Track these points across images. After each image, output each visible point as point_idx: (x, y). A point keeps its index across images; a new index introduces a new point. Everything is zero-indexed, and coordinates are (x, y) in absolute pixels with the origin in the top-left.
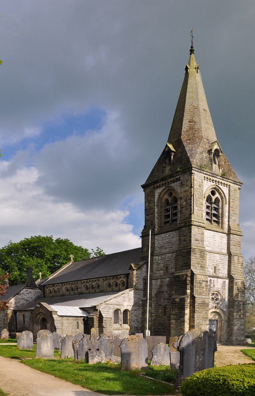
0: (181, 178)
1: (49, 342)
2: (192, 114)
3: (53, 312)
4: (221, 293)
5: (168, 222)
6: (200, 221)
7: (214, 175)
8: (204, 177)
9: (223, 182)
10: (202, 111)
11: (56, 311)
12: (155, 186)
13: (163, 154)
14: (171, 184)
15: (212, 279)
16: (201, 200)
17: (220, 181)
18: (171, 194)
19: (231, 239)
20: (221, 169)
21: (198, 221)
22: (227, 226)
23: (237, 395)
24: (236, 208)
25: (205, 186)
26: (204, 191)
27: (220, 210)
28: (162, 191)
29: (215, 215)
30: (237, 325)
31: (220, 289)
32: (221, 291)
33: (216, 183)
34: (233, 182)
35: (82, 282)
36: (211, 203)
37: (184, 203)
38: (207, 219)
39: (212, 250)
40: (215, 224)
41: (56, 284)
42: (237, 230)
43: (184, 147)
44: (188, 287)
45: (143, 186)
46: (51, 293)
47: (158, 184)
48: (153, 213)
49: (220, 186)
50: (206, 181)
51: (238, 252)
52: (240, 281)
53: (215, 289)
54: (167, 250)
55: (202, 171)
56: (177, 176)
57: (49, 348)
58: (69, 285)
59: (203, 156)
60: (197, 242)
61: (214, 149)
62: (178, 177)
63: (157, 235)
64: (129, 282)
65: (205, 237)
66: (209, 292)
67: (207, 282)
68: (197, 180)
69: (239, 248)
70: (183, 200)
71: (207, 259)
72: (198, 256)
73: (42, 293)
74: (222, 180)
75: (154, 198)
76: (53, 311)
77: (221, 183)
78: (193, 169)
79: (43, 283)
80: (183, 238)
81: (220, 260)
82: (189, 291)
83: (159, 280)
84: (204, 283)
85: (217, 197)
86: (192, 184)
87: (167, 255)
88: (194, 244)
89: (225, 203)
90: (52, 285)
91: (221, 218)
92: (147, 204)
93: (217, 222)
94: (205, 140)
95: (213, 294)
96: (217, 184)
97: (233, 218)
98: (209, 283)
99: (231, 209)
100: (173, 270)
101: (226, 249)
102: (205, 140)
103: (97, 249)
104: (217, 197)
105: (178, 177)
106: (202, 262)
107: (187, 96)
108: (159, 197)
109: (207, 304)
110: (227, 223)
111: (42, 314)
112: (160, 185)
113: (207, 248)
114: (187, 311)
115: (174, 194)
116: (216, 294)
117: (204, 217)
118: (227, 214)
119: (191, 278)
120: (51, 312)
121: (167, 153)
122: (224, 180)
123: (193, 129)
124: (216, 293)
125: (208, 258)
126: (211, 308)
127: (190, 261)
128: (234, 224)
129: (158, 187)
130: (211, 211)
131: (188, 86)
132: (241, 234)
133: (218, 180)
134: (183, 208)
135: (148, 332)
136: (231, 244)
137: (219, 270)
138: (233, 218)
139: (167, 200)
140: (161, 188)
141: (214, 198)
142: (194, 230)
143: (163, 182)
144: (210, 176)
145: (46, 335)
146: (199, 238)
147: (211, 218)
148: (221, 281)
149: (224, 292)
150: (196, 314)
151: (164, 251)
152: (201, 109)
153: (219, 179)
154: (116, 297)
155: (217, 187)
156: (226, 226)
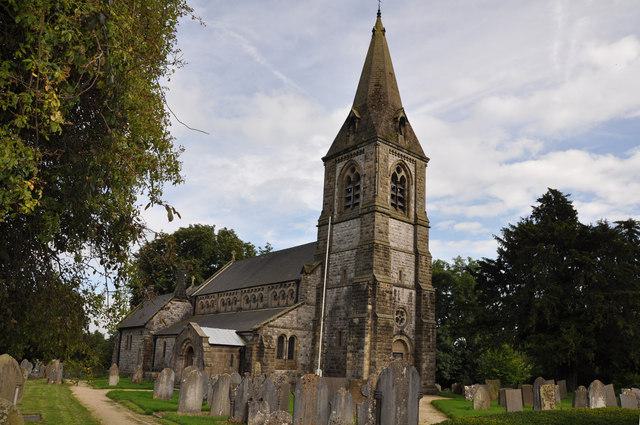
1: (198, 385)
9: (410, 156)
40: (400, 211)
45: (324, 159)
84: (388, 295)
100: (352, 275)
113: (391, 244)
118: (413, 198)
120: (202, 337)
129: (340, 161)
139: (349, 177)
142: (379, 218)
148: (407, 291)
151: (343, 247)
156: (412, 214)
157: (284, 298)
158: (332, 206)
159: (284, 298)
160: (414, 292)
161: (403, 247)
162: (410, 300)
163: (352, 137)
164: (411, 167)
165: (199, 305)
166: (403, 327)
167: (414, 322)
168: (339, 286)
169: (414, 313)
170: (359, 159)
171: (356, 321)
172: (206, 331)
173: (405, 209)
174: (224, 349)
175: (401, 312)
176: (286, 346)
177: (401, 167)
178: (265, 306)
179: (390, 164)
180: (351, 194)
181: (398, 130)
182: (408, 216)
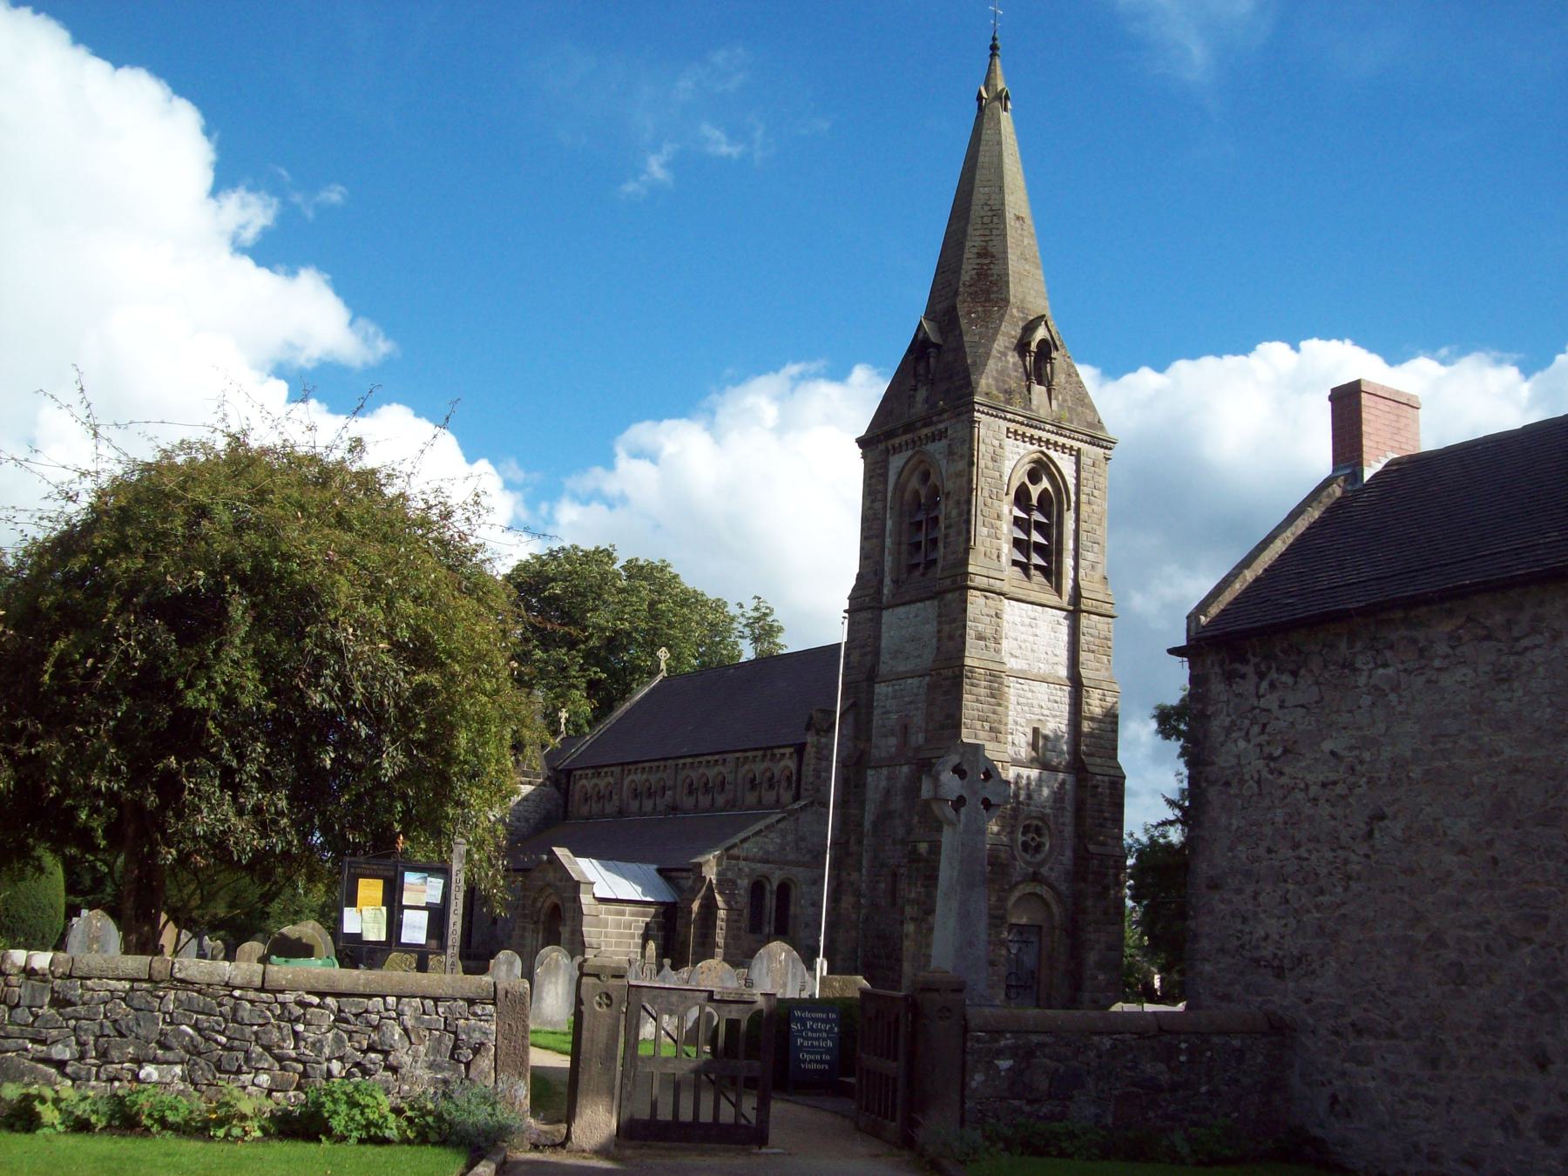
0: (949, 432)
1: (560, 981)
2: (987, 232)
3: (582, 886)
4: (1051, 824)
5: (918, 565)
6: (992, 573)
7: (1035, 423)
8: (1008, 429)
9: (1061, 440)
10: (1012, 223)
11: (592, 880)
12: (890, 443)
13: (911, 350)
14: (926, 444)
17: (1053, 438)
18: (926, 477)
19: (1083, 629)
20: (1057, 399)
21: (985, 572)
24: (1098, 522)
25: (1010, 456)
26: (1007, 472)
28: (906, 463)
31: (1048, 811)
32: (1051, 818)
33: (1040, 446)
34: (1088, 439)
35: (680, 766)
36: (1027, 508)
37: (954, 513)
38: (1015, 563)
39: (1025, 667)
41: (605, 766)
42: (1100, 597)
43: (961, 335)
45: (862, 442)
46: (586, 800)
47: (897, 441)
49: (1051, 453)
51: (1103, 674)
52: (1106, 779)
55: (1001, 414)
56: (940, 422)
57: (560, 1000)
58: (642, 773)
59: (1007, 362)
60: (982, 643)
61: (1037, 340)
62: (941, 426)
63: (887, 608)
64: (803, 777)
65: (1005, 624)
66: (1012, 821)
68: (987, 440)
69: (1105, 658)
70: (951, 502)
71: (1012, 701)
72: (983, 691)
73: (560, 801)
74: (1057, 434)
76: (582, 880)
77: (1056, 444)
79: (567, 761)
80: (946, 628)
83: (885, 771)
85: (1046, 490)
86: (973, 455)
87: (910, 681)
88: (974, 656)
89: (1065, 507)
90: (592, 771)
94: (1015, 311)
96: (1044, 449)
97: (1090, 556)
99: (1083, 526)
100: (921, 738)
102: (1015, 311)
103: (754, 603)
105: (941, 426)
106: (994, 712)
107: (977, 177)
108: (897, 484)
110: (1071, 574)
111: (551, 891)
112: (900, 444)
113: (1012, 664)
115: (933, 479)
117: (1004, 559)
120: (578, 883)
122: (1061, 435)
123: (987, 275)
124: (1035, 822)
125: (1013, 699)
126: (1019, 879)
128: (1092, 576)
129: (897, 450)
131: (981, 148)
132: (1112, 613)
133: (1045, 435)
138: (1088, 557)
139: (917, 494)
141: (1035, 491)
143: (908, 437)
144: (1022, 424)
145: (557, 961)
146: (989, 632)
151: (902, 667)
152: (1010, 216)
153: (1048, 431)
154: (761, 831)
155: (1045, 459)
156: (1068, 584)
157: (771, 787)
158: (880, 563)
159: (771, 787)
160: (1070, 779)
161: (1044, 668)
163: (922, 394)
164: (1066, 464)
165: (576, 795)
166: (1042, 863)
167: (1069, 853)
169: (1069, 831)
170: (936, 448)
171: (923, 847)
172: (587, 868)
173: (1052, 573)
174: (628, 909)
176: (770, 902)
178: (731, 804)
180: (922, 537)
182: (1058, 590)
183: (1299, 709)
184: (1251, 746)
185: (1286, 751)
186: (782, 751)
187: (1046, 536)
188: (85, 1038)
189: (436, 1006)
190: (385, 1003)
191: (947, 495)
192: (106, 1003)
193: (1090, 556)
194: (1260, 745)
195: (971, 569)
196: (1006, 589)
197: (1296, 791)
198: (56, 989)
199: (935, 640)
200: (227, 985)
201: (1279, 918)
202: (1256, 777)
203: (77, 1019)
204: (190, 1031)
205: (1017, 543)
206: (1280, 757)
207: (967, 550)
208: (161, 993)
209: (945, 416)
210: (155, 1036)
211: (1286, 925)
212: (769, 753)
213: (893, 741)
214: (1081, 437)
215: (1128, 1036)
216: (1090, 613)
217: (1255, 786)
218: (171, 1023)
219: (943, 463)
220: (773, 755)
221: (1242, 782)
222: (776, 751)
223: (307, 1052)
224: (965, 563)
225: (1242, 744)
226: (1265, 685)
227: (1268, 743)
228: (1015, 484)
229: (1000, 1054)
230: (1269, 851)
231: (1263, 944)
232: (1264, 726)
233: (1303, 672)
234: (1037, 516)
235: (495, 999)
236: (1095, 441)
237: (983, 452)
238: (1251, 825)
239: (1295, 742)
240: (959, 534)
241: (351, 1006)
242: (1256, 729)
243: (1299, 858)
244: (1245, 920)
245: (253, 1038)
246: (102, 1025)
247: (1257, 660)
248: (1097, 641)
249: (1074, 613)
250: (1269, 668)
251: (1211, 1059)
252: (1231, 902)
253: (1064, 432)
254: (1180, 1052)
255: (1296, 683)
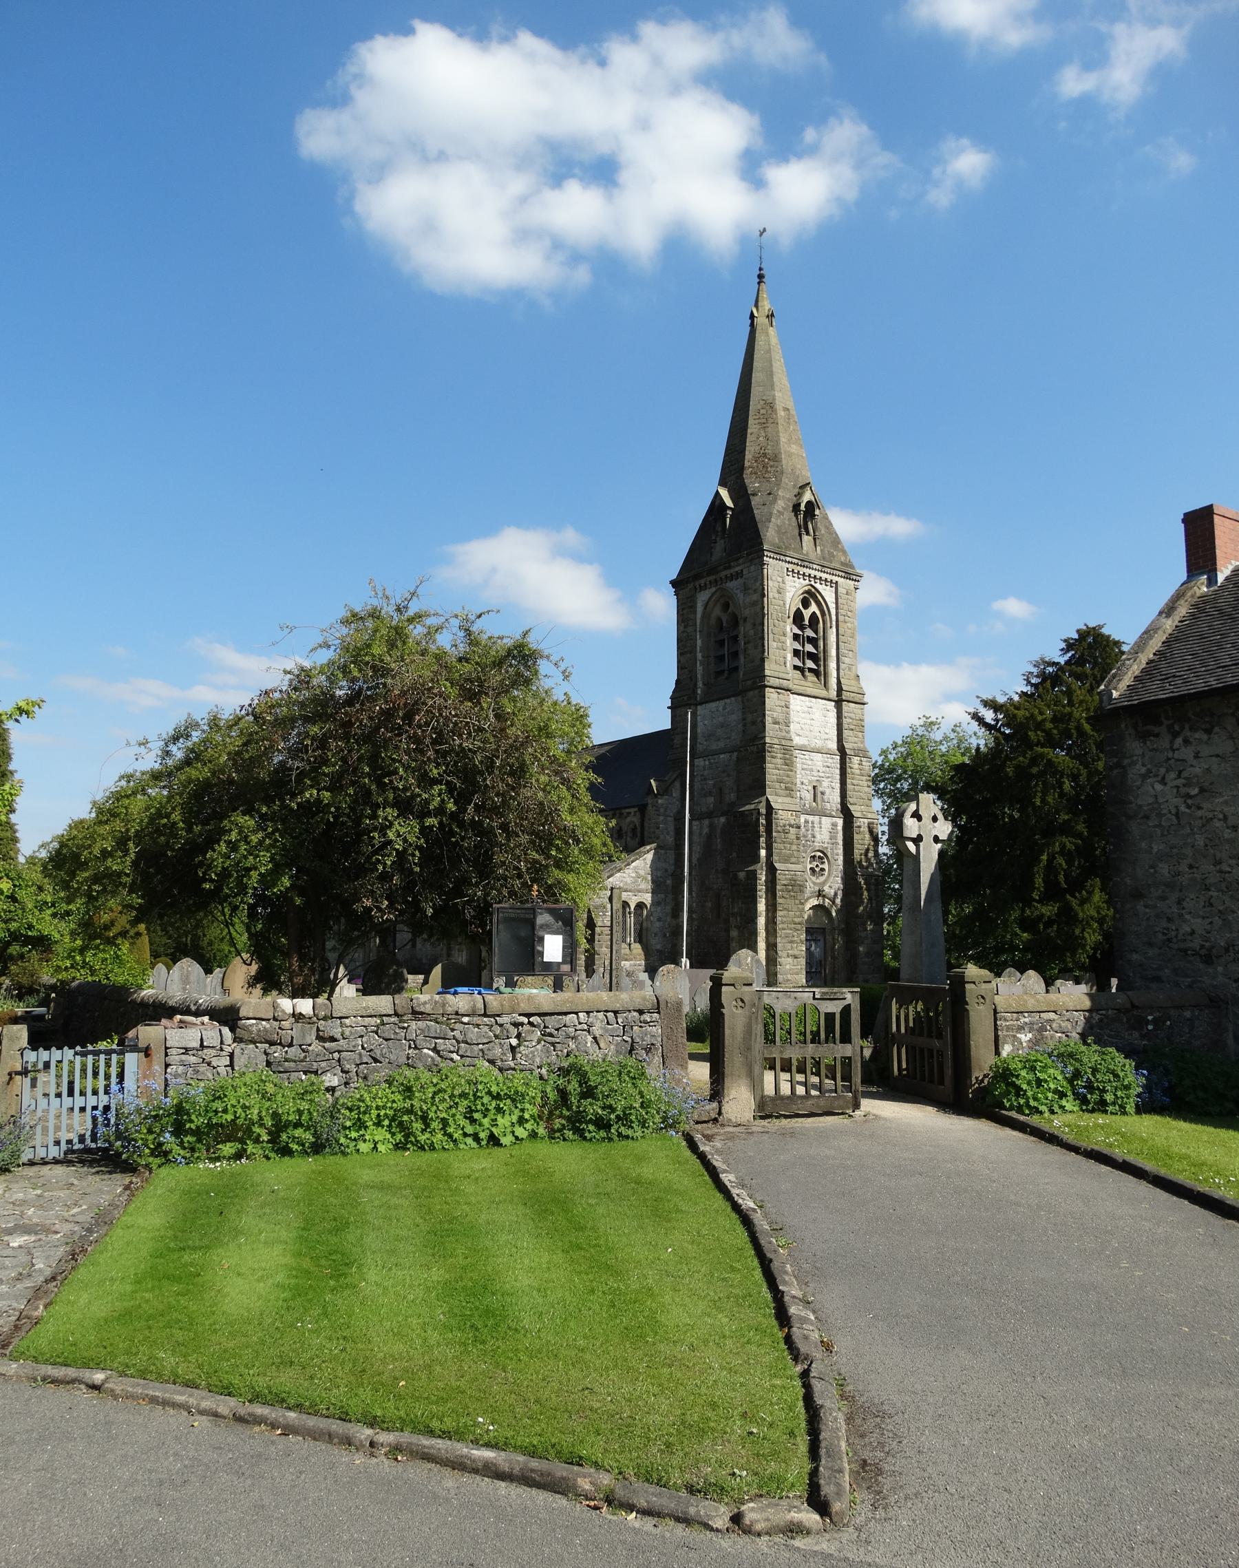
2: (764, 421)
4: (829, 855)
5: (723, 671)
6: (781, 675)
9: (824, 576)
12: (697, 584)
15: (810, 818)
16: (781, 623)
17: (819, 574)
18: (726, 606)
19: (845, 714)
21: (776, 674)
22: (835, 680)
23: (216, 1566)
27: (821, 643)
28: (710, 598)
29: (811, 656)
30: (866, 942)
34: (843, 574)
36: (802, 627)
37: (752, 632)
38: (796, 668)
39: (807, 743)
40: (811, 677)
44: (762, 840)
45: (674, 583)
48: (693, 651)
49: (818, 586)
50: (791, 577)
53: (817, 845)
54: (721, 745)
55: (782, 557)
62: (737, 569)
63: (701, 704)
64: (646, 829)
67: (799, 827)
68: (774, 578)
72: (779, 761)
75: (695, 613)
78: (766, 553)
81: (824, 769)
82: (763, 853)
84: (793, 831)
85: (814, 613)
87: (722, 756)
88: (772, 734)
91: (822, 663)
92: (682, 628)
93: (816, 673)
95: (814, 857)
96: (813, 583)
98: (803, 829)
100: (733, 796)
101: (835, 738)
104: (689, 1040)
105: (737, 569)
106: (788, 776)
108: (704, 613)
109: (800, 886)
110: (834, 674)
113: (797, 741)
114: (762, 906)
116: (819, 857)
117: (788, 665)
118: (833, 652)
119: (766, 820)
121: (717, 507)
124: (819, 854)
127: (764, 774)
130: (803, 647)
133: (813, 573)
134: (749, 642)
135: (685, 961)
136: (845, 726)
137: (823, 793)
139: (719, 620)
140: (707, 592)
141: (807, 614)
142: (771, 698)
143: (712, 578)
144: (798, 564)
146: (781, 718)
147: (804, 663)
148: (826, 821)
149: (835, 851)
150: (779, 913)
151: (714, 746)
158: (693, 671)
161: (818, 743)
162: (833, 837)
164: (828, 594)
166: (824, 883)
168: (709, 815)
175: (822, 856)
177: (810, 596)
179: (789, 596)
181: (803, 528)
183: (1214, 758)
184: (1168, 787)
185: (1202, 790)
186: (628, 810)
187: (816, 647)
188: (348, 1066)
189: (616, 1018)
190: (578, 1018)
191: (745, 620)
192: (362, 1036)
193: (846, 660)
194: (1178, 787)
195: (767, 672)
196: (791, 686)
197: (1216, 820)
198: (322, 1028)
199: (740, 726)
200: (457, 1013)
201: (1203, 918)
202: (1174, 811)
203: (339, 1052)
204: (431, 1053)
205: (796, 653)
206: (1196, 795)
207: (763, 660)
208: (406, 1025)
209: (741, 561)
210: (403, 1060)
211: (1211, 923)
212: (618, 812)
213: (711, 800)
214: (838, 573)
215: (1110, 1012)
216: (848, 701)
217: (1174, 817)
218: (416, 1048)
219: (741, 596)
220: (621, 814)
221: (1160, 815)
222: (623, 811)
223: (523, 1062)
224: (761, 667)
225: (1159, 787)
226: (1179, 740)
227: (1184, 785)
228: (793, 610)
229: (1021, 1029)
230: (1191, 867)
231: (1189, 938)
232: (1180, 772)
233: (1216, 729)
234: (809, 633)
235: (658, 1008)
236: (848, 576)
237: (771, 586)
238: (1171, 848)
239: (1212, 784)
240: (756, 647)
241: (552, 1022)
242: (1172, 775)
243: (1221, 871)
244: (1169, 920)
245: (481, 1054)
246: (360, 1055)
247: (1170, 722)
248: (855, 722)
249: (839, 703)
250: (1182, 729)
251: (1170, 1027)
252: (1155, 907)
253: (826, 570)
254: (1148, 1022)
255: (1209, 739)
